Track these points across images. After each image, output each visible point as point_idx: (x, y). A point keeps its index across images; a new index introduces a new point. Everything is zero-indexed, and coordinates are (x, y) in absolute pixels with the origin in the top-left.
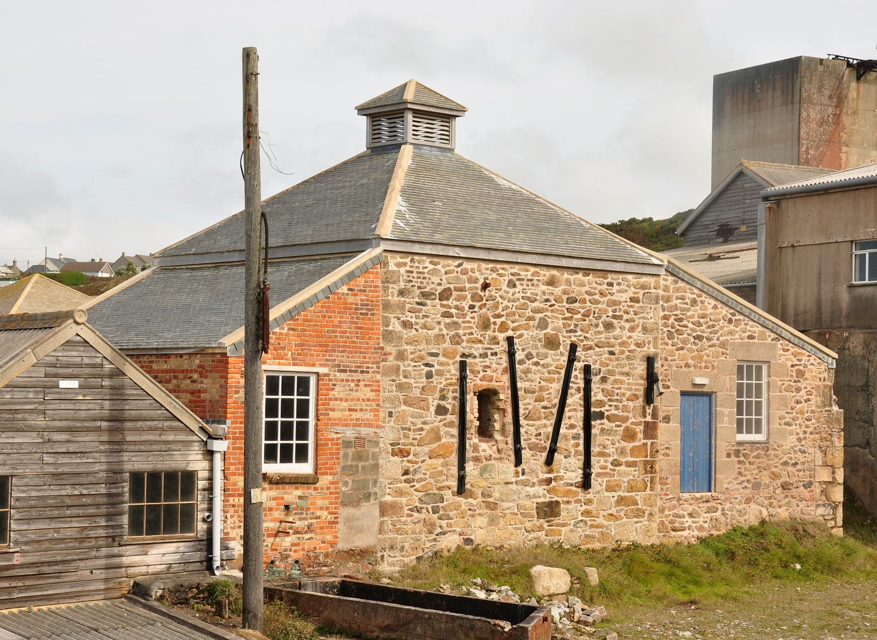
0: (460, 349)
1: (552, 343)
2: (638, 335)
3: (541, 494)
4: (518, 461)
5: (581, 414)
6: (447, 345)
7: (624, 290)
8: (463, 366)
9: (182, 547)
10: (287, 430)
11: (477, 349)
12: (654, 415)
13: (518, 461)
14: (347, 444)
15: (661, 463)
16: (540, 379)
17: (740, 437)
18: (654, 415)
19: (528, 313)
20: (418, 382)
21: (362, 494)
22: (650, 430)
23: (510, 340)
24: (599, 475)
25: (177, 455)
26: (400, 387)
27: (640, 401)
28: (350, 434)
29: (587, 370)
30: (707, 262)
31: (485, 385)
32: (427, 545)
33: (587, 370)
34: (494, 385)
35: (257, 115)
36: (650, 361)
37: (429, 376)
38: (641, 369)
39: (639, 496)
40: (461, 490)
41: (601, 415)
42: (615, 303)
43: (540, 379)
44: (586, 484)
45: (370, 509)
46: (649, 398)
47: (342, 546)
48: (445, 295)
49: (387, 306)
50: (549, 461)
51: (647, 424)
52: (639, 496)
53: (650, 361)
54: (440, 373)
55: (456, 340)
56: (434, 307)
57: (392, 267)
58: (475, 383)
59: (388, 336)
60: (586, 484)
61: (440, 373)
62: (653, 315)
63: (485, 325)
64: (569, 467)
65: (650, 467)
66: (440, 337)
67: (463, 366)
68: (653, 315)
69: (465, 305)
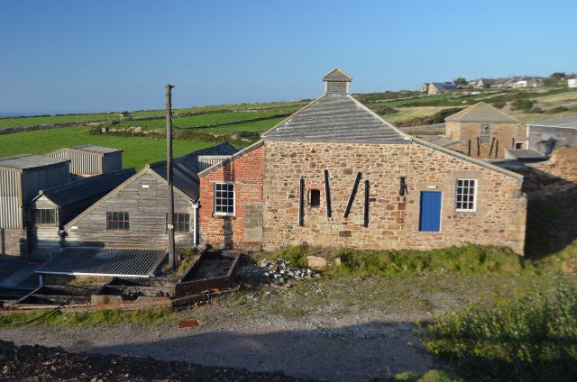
0: (301, 174)
1: (349, 172)
2: (396, 168)
3: (342, 228)
4: (330, 215)
5: (364, 199)
6: (295, 173)
7: (388, 149)
8: (302, 181)
9: (185, 236)
10: (225, 195)
11: (308, 175)
12: (405, 200)
13: (330, 215)
14: (247, 207)
15: (407, 219)
16: (341, 185)
17: (458, 210)
18: (405, 200)
19: (337, 161)
20: (280, 186)
21: (253, 224)
22: (402, 206)
23: (326, 172)
24: (372, 222)
25: (183, 208)
26: (273, 188)
27: (397, 195)
28: (249, 204)
29: (367, 182)
30: (496, 77)
31: (314, 188)
32: (285, 243)
33: (367, 182)
34: (317, 188)
35: (211, 107)
36: (403, 179)
37: (286, 184)
38: (398, 182)
39: (395, 232)
40: (302, 223)
41: (374, 200)
42: (383, 156)
43: (341, 185)
44: (366, 225)
45: (258, 230)
46: (402, 193)
47: (245, 240)
48: (293, 155)
49: (265, 160)
50: (346, 216)
51: (400, 204)
52: (395, 232)
53: (403, 179)
54: (291, 184)
55: (299, 171)
56: (288, 161)
57: (269, 146)
58: (308, 187)
59: (266, 171)
60: (366, 225)
61: (291, 184)
62: (406, 160)
63: (313, 165)
64: (357, 218)
65: (402, 221)
66: (292, 171)
67: (302, 181)
68: (406, 160)
69: (304, 159)
